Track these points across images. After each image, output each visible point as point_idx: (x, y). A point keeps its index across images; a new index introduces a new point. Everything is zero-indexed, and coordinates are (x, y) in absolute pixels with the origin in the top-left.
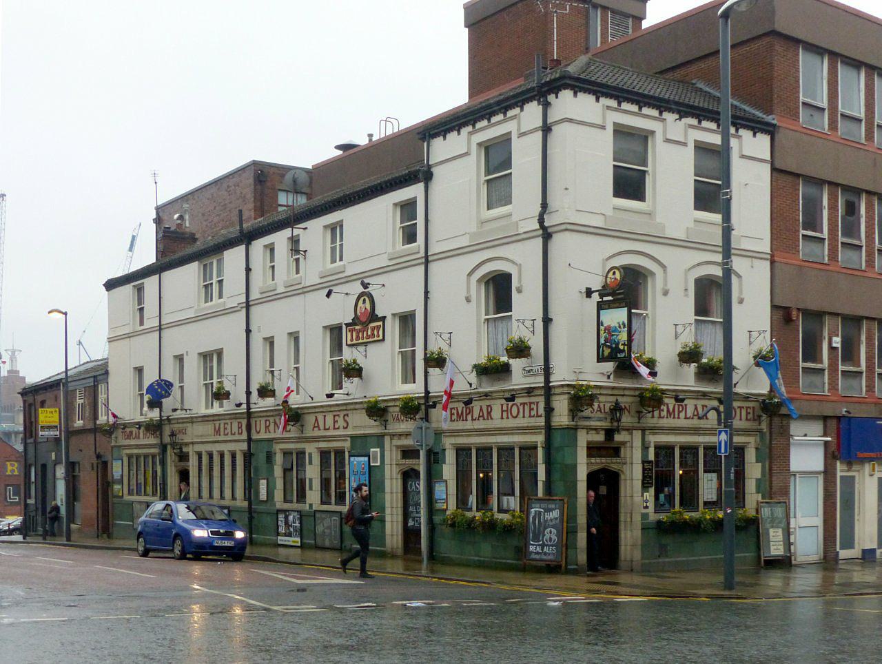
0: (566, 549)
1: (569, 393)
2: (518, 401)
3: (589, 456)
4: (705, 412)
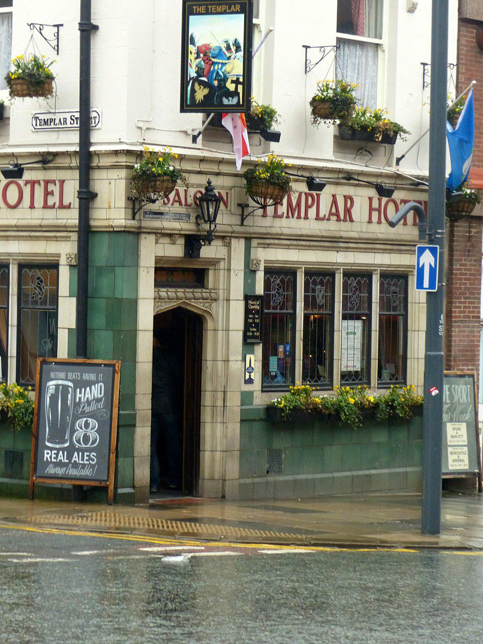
0: (117, 457)
1: (128, 167)
2: (27, 176)
3: (158, 284)
4: (400, 213)
